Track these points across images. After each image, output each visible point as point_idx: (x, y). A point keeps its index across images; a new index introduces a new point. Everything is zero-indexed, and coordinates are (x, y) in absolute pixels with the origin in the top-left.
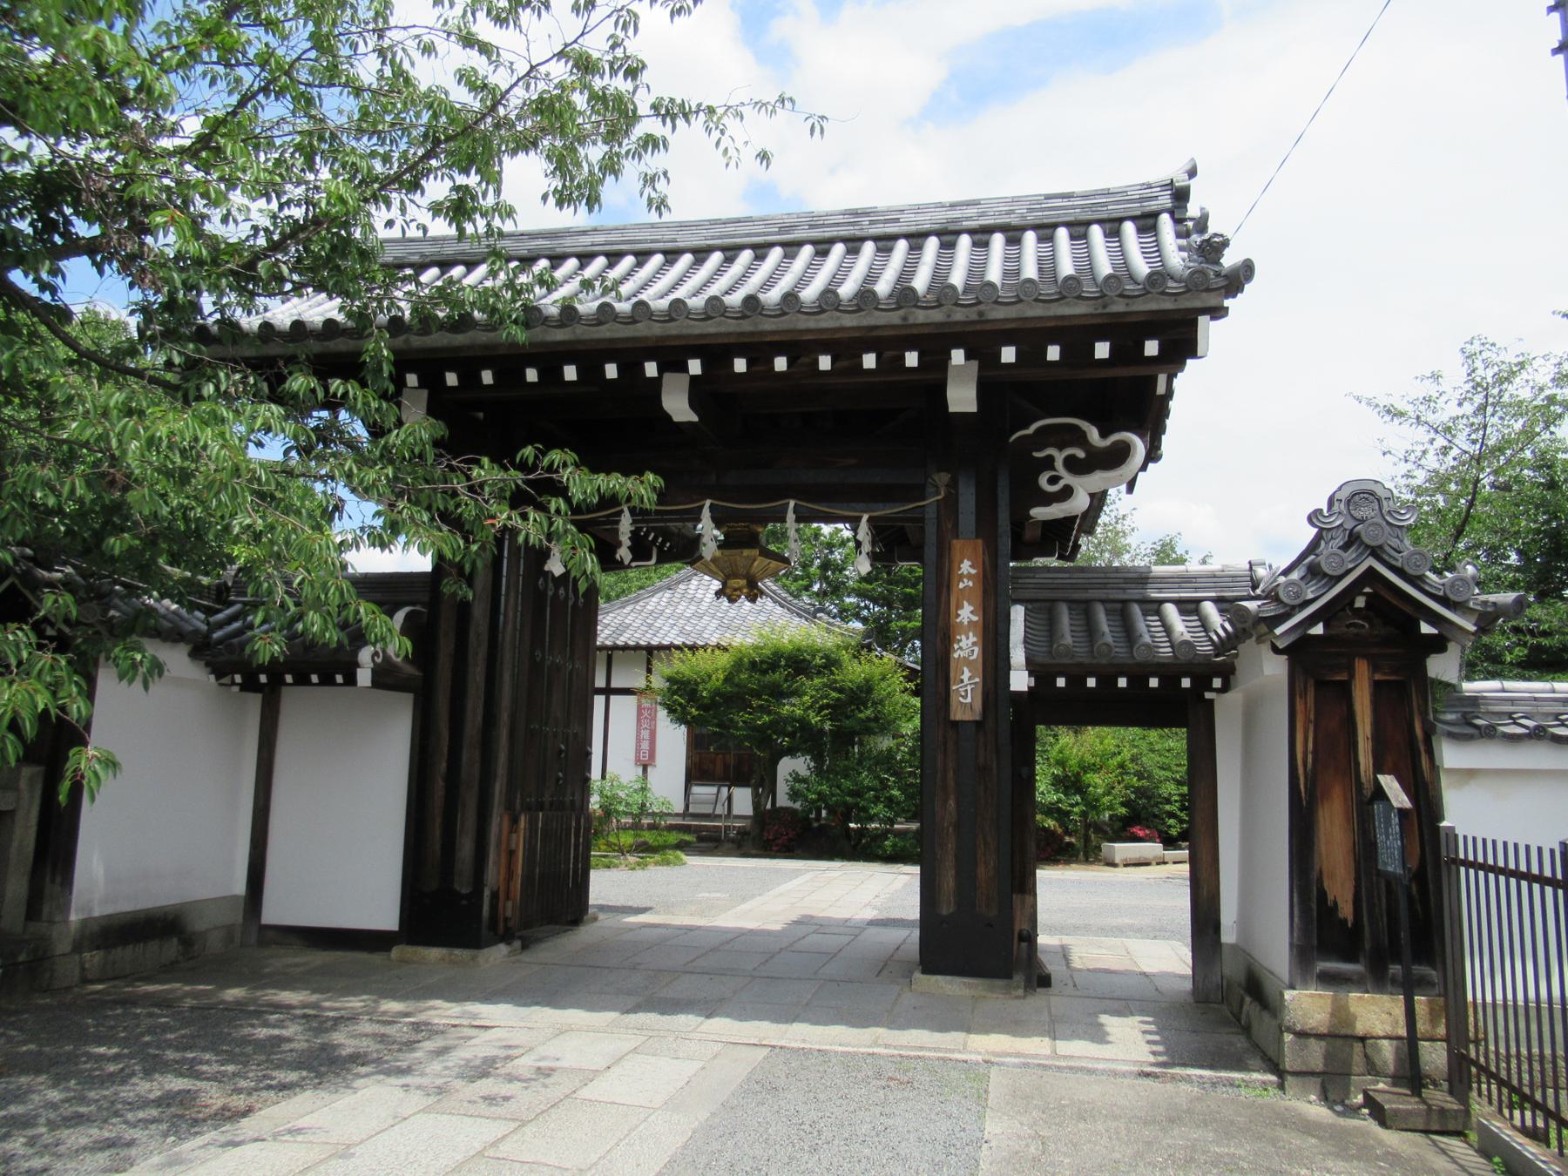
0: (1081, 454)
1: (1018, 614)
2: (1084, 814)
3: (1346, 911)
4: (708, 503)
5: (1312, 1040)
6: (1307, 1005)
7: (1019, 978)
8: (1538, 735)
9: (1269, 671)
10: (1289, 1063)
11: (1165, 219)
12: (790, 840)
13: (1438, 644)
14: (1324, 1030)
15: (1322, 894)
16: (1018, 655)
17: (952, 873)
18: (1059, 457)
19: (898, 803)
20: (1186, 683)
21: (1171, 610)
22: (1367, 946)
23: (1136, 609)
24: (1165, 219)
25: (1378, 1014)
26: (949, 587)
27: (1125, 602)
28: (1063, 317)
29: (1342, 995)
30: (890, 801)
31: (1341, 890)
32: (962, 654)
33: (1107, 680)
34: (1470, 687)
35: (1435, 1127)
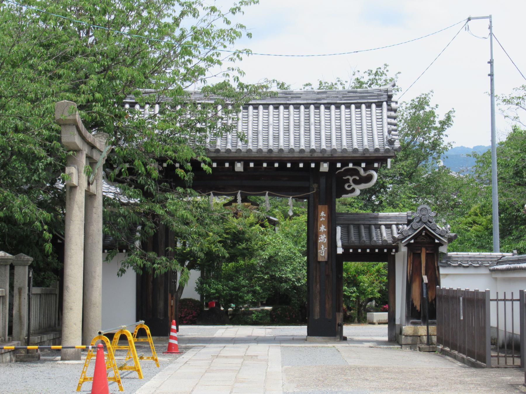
0: (358, 178)
1: (339, 229)
2: (358, 297)
3: (418, 308)
4: (239, 191)
5: (409, 337)
6: (408, 329)
7: (338, 337)
8: (460, 266)
9: (404, 249)
10: (403, 342)
11: (385, 103)
12: (194, 317)
13: (441, 244)
14: (411, 335)
15: (413, 304)
16: (339, 243)
17: (318, 306)
18: (351, 179)
19: (259, 293)
20: (385, 251)
21: (383, 227)
22: (422, 315)
23: (373, 227)
24: (385, 103)
25: (422, 330)
26: (317, 220)
27: (370, 225)
28: (354, 157)
29: (416, 327)
30: (254, 292)
31: (417, 303)
32: (322, 241)
33: (364, 250)
34: (449, 254)
35: (431, 350)
